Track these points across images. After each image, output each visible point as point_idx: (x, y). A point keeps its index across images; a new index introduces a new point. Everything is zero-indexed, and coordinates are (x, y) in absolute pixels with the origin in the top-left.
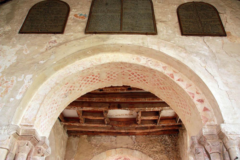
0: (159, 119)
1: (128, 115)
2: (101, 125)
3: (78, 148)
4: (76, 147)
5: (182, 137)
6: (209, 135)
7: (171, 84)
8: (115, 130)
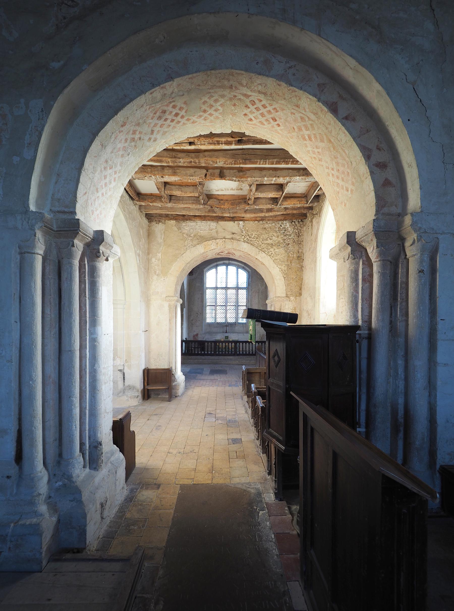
0: (281, 196)
1: (234, 190)
2: (194, 205)
3: (164, 238)
4: (161, 237)
5: (310, 224)
6: (383, 231)
7: (329, 126)
8: (215, 213)
